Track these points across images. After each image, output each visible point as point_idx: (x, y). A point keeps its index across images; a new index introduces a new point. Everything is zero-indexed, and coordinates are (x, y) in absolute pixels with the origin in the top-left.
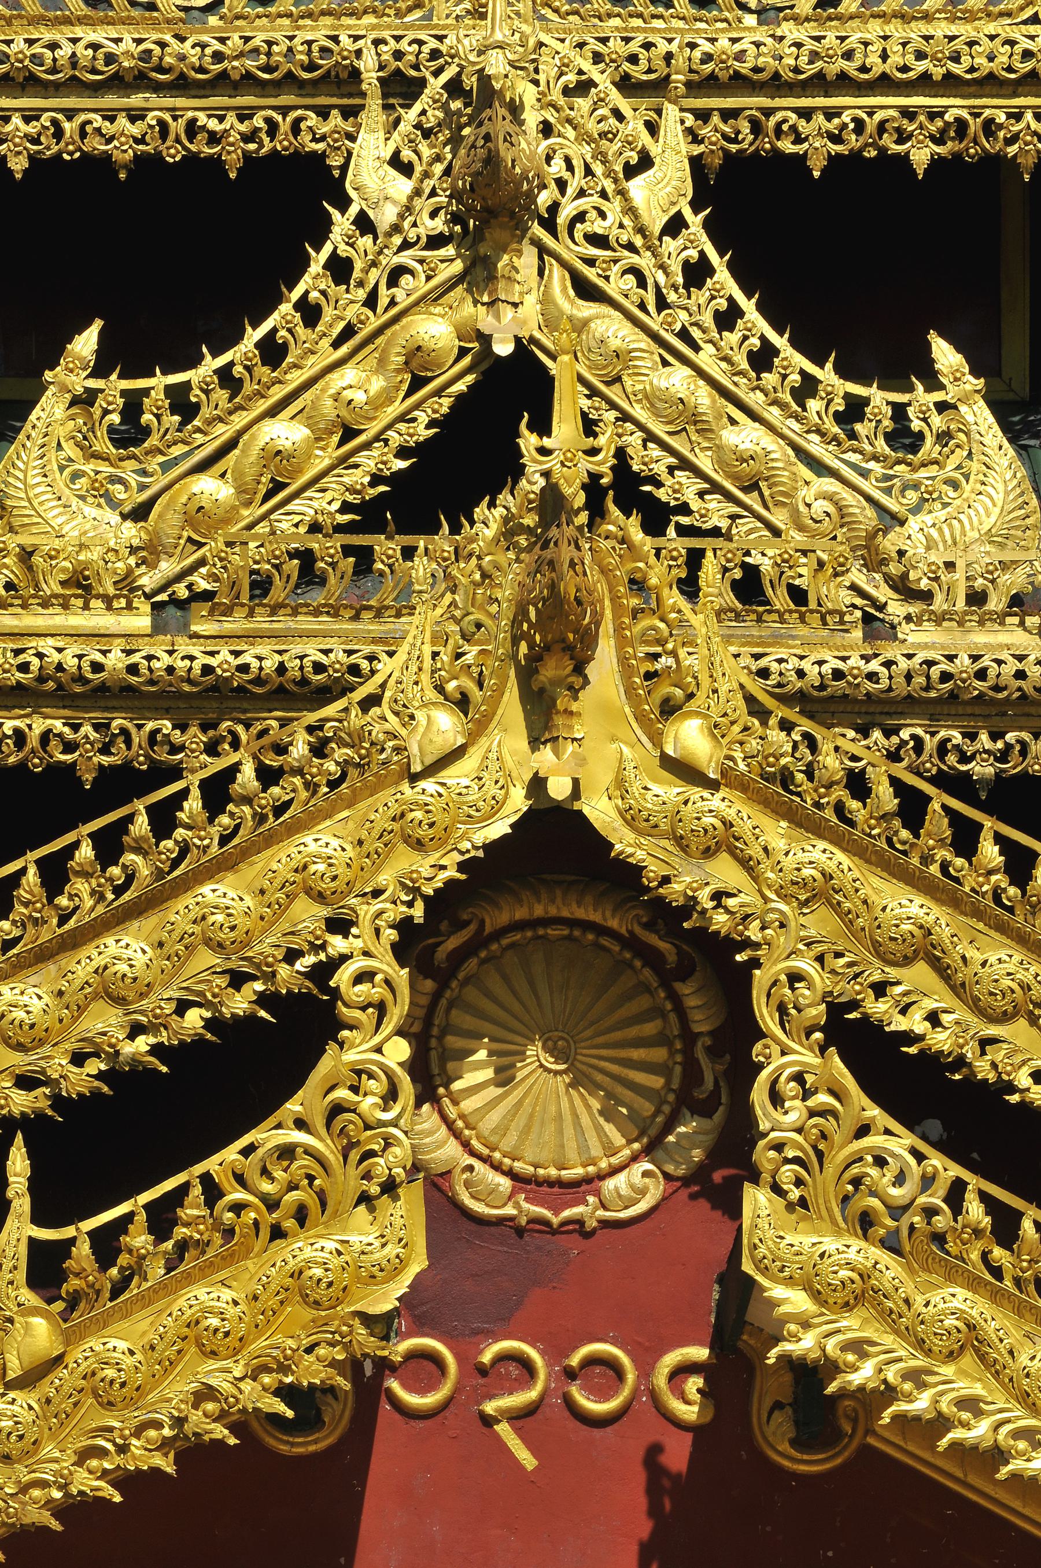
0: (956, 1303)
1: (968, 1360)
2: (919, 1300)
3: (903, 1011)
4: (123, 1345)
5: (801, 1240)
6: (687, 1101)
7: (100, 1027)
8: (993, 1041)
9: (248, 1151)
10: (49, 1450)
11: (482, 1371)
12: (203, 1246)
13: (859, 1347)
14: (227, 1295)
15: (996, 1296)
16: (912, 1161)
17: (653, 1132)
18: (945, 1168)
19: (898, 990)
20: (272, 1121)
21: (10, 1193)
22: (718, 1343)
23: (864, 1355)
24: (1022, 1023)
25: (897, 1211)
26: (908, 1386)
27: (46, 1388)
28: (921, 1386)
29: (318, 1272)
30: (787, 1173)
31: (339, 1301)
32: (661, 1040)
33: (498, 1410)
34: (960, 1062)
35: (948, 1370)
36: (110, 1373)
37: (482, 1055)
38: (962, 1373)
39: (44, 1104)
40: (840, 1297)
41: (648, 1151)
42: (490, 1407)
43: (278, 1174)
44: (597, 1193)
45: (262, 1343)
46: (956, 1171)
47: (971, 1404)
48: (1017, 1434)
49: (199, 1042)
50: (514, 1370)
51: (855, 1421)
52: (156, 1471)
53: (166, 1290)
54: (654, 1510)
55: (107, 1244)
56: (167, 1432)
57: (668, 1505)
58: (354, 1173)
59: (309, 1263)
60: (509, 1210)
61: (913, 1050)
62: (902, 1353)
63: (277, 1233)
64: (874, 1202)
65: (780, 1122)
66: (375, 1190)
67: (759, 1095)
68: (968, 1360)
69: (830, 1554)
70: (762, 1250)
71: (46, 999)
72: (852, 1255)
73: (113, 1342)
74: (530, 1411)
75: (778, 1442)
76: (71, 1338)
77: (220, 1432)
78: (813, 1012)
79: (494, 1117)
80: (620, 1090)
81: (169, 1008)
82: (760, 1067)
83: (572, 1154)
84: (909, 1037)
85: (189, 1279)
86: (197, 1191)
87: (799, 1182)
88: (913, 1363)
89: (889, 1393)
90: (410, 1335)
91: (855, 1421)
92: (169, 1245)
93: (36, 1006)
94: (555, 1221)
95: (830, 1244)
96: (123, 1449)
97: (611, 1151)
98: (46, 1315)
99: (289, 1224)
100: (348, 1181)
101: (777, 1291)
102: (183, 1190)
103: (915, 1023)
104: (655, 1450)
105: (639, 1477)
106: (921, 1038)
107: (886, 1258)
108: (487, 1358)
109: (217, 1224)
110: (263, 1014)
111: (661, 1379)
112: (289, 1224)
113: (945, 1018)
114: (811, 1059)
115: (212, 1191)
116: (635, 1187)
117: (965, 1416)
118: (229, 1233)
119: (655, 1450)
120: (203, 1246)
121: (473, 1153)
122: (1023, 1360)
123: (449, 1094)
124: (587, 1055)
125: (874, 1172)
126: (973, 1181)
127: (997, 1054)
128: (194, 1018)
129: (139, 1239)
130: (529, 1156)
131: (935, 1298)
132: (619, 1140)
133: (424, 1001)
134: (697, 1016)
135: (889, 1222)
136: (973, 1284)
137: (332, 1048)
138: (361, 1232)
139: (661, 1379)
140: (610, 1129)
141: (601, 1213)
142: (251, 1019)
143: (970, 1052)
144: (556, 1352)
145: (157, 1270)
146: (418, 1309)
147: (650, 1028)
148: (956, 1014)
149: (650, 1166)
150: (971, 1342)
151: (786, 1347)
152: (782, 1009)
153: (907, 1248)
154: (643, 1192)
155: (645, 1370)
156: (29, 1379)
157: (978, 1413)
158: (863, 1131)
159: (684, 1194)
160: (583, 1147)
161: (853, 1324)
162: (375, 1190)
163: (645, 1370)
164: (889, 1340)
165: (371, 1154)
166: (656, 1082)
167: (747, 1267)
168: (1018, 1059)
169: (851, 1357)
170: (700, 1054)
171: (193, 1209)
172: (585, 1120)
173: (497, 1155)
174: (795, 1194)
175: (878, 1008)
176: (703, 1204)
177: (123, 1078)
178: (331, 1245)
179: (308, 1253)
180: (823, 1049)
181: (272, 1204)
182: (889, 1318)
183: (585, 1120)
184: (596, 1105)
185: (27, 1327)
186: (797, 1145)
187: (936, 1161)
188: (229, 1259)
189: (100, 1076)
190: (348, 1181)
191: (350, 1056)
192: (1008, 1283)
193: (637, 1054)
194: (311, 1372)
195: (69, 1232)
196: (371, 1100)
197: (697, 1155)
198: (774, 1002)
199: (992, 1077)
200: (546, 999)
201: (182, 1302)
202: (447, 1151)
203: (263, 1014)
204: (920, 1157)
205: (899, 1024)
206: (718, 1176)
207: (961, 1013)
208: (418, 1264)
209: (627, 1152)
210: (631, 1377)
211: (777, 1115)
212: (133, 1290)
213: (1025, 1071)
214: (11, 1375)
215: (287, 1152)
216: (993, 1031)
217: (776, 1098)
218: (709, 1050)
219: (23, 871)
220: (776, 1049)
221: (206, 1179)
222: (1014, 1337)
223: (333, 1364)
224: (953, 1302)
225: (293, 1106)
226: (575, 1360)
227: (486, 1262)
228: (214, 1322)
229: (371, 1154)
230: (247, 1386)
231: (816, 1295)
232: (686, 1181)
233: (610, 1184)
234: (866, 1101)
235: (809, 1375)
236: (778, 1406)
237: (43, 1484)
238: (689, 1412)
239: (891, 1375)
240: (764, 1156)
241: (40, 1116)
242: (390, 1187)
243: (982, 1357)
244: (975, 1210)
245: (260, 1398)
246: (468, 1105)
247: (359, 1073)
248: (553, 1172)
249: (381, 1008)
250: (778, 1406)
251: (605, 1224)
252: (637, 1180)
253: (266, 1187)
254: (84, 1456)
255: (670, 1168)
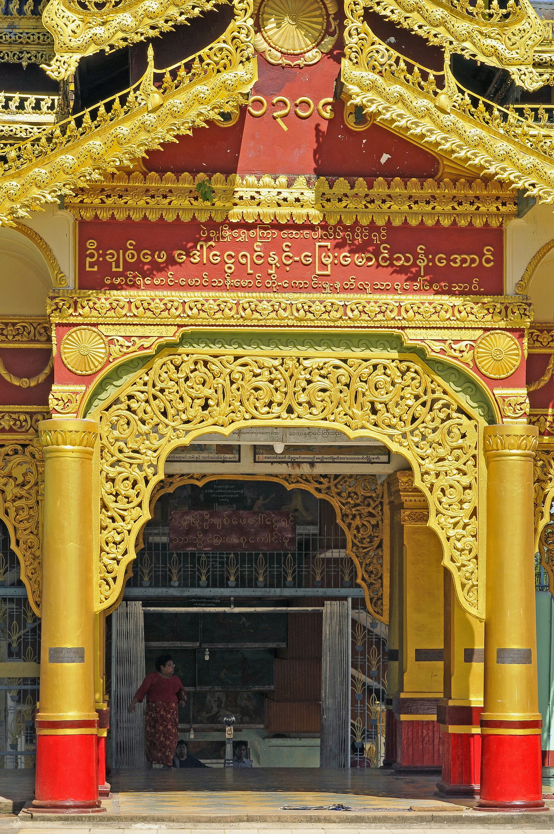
0: (397, 89)
1: (400, 104)
2: (387, 89)
3: (384, 10)
4: (178, 101)
5: (357, 73)
6: (328, 32)
7: (172, 13)
8: (408, 17)
9: (211, 49)
10: (160, 129)
11: (273, 105)
12: (199, 75)
13: (371, 101)
14: (206, 88)
15: (407, 87)
16: (386, 52)
17: (318, 41)
18: (395, 54)
19: (383, 4)
20: (217, 41)
21: (148, 60)
22: (335, 96)
23: (373, 103)
24: (416, 13)
25: (382, 65)
26: (384, 111)
27: (158, 113)
28: (388, 111)
29: (229, 82)
30: (353, 55)
31: (235, 90)
32: (321, 16)
33: (278, 115)
34: (399, 23)
35: (395, 107)
36: (175, 109)
37: (273, 20)
38: (399, 107)
39: (158, 34)
40: (367, 88)
41: (317, 46)
42: (275, 114)
43: (219, 55)
44: (304, 57)
45: (215, 101)
46: (397, 54)
47: (401, 116)
48: (412, 123)
49: (198, 17)
50: (282, 104)
51: (371, 117)
52: (188, 135)
53: (189, 87)
54: (317, 141)
55: (174, 74)
56: (190, 125)
57: (321, 139)
58: (239, 55)
59: (227, 80)
60: (280, 62)
61: (387, 20)
62: (383, 102)
63: (219, 71)
64: (376, 63)
65: (351, 41)
66: (244, 60)
67: (346, 34)
68: (400, 104)
69: (364, 141)
70: (346, 76)
71: (158, 5)
72: (370, 77)
73: (176, 101)
74: (286, 115)
75: (350, 122)
76: (164, 100)
77: (204, 125)
78: (360, 12)
79: (276, 37)
80: (310, 29)
81: (190, 7)
82: (346, 27)
83: (297, 47)
84: (386, 17)
85: (196, 84)
86: (197, 60)
87: (356, 58)
88: (386, 105)
89: (379, 113)
90: (254, 95)
91: (371, 117)
92: (190, 74)
93: (155, 7)
94: (293, 65)
95: (364, 74)
96: (179, 129)
97: (307, 46)
98: (158, 93)
99: (222, 69)
100: (237, 57)
101: (350, 86)
102: (194, 59)
103: (387, 13)
104: (318, 125)
105: (314, 132)
106: (389, 17)
107: (378, 77)
108: (274, 101)
109: (203, 69)
110: (215, 9)
111: (320, 107)
112: (222, 69)
113: (395, 11)
114: (360, 24)
115: (201, 60)
116: (314, 56)
117: (399, 119)
118: (206, 72)
119: (318, 125)
120: (199, 75)
121: (271, 46)
122: (414, 104)
123: (265, 31)
124: (301, 20)
125: (376, 55)
126: (402, 57)
127: (409, 21)
128: (197, 11)
129: (182, 72)
130: (286, 48)
131: (392, 88)
132: (309, 43)
133: (257, 8)
134: (330, 9)
135: (380, 68)
136: (402, 84)
137: (233, 20)
138: (240, 70)
139: (320, 107)
140: (307, 39)
141: (305, 63)
142: (212, 11)
143: (402, 20)
144: (293, 99)
145: (187, 81)
146: (257, 89)
147: (318, 13)
148: (398, 10)
149: (317, 50)
150: (401, 99)
151: (352, 101)
152: (352, 11)
153: (384, 75)
154: (316, 57)
155: (316, 104)
156: (154, 111)
157: (402, 118)
158: (373, 44)
159: (326, 57)
160: (300, 45)
161: (370, 95)
162: (244, 60)
163: (316, 104)
164: (379, 99)
165: (244, 50)
166: (319, 27)
167: (342, 80)
168: (414, 22)
169: (369, 104)
170: (331, 19)
171: (196, 64)
172: (300, 37)
173: (277, 47)
174: (355, 61)
175: (377, 9)
176: (331, 60)
177: (178, 27)
178: (233, 75)
179: (227, 77)
180: (363, 22)
181: (217, 63)
182: (380, 93)
183: (300, 37)
184: (303, 33)
185: (153, 96)
186: (356, 48)
187: (392, 51)
188: (206, 78)
189: (172, 26)
190: (237, 57)
191: (238, 23)
192: (411, 83)
193: (314, 20)
194: (227, 109)
195: (163, 71)
196: (243, 35)
197: (330, 47)
198: (350, 9)
199: (408, 27)
200: (290, 5)
201: (193, 90)
202: (263, 46)
203: (215, 9)
204: (388, 51)
205: (383, 13)
206: (335, 53)
207: (400, 10)
208: (256, 79)
209: (311, 46)
210: (312, 106)
211: (351, 40)
212: (181, 87)
213: (416, 25)
214: (149, 109)
215: (221, 49)
216: (408, 15)
217: (350, 35)
218: (333, 18)
219: (129, 92)
220: (350, 22)
221: (200, 56)
222: (412, 98)
223: (233, 106)
224: (396, 89)
225: (222, 37)
226: (298, 102)
227: (275, 75)
228: (202, 95)
229: (244, 50)
230: (211, 112)
231: (360, 87)
232: (327, 54)
233: (307, 55)
234: (374, 36)
235: (359, 109)
236: (351, 113)
237: (159, 139)
238: (327, 115)
239: (380, 108)
240: (347, 51)
241: (157, 37)
242: (248, 59)
243: (404, 103)
244: (402, 65)
245: (214, 115)
246: (269, 33)
247: (240, 28)
248: (292, 52)
249: (246, 10)
250: (351, 113)
251: (306, 65)
252: (315, 54)
253: (215, 59)
254: (168, 131)
255: (322, 51)
